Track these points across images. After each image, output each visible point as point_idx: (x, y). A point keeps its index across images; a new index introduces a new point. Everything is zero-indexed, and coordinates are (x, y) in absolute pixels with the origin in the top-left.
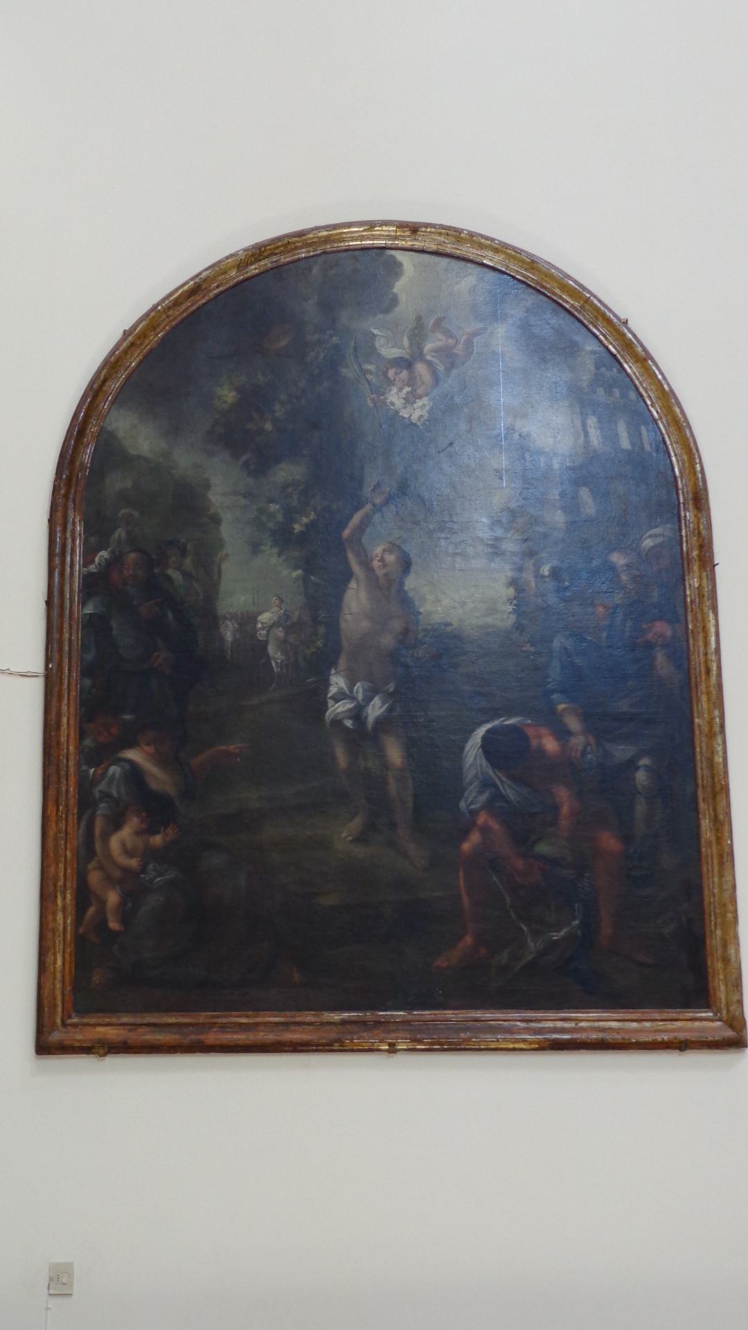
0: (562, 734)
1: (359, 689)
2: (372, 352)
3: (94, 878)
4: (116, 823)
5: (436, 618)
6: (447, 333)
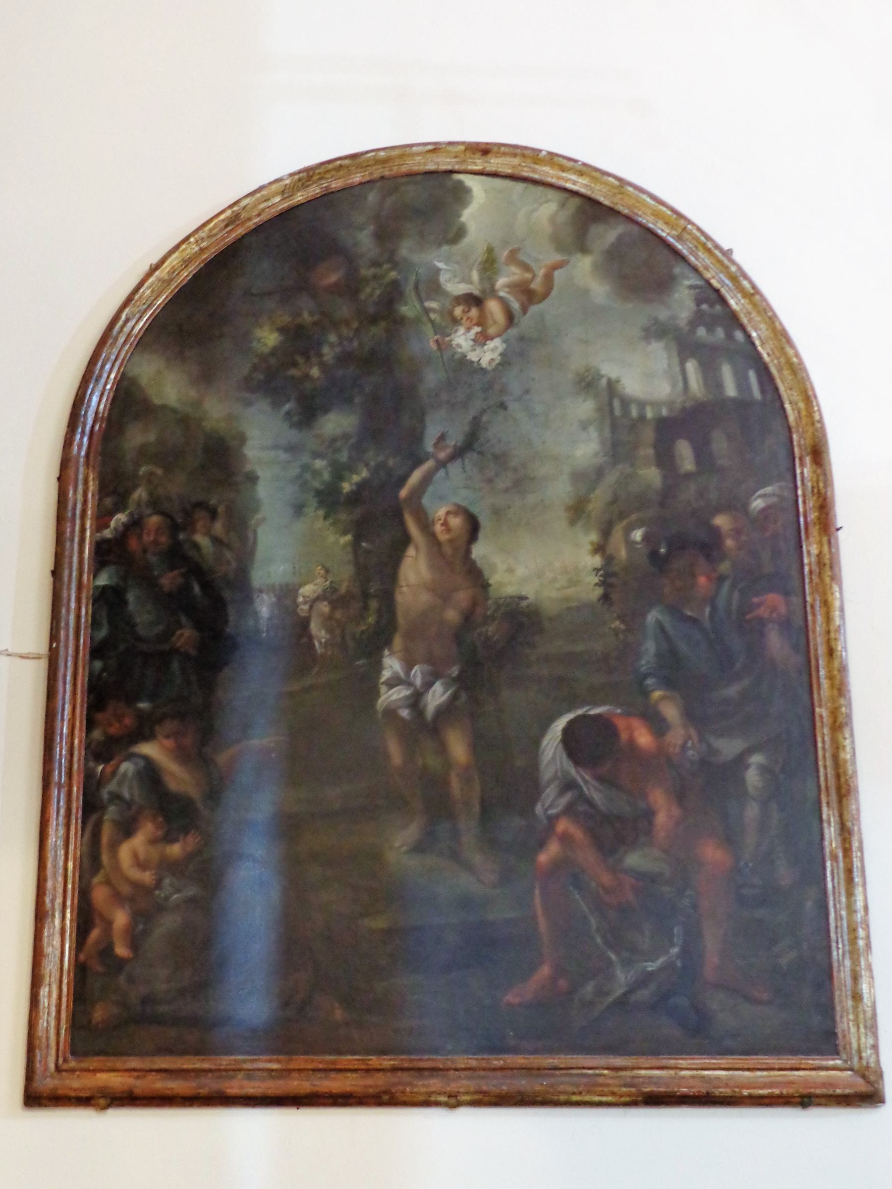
0: (658, 725)
1: (418, 674)
2: (435, 288)
3: (100, 895)
4: (127, 830)
5: (511, 590)
6: (526, 268)
